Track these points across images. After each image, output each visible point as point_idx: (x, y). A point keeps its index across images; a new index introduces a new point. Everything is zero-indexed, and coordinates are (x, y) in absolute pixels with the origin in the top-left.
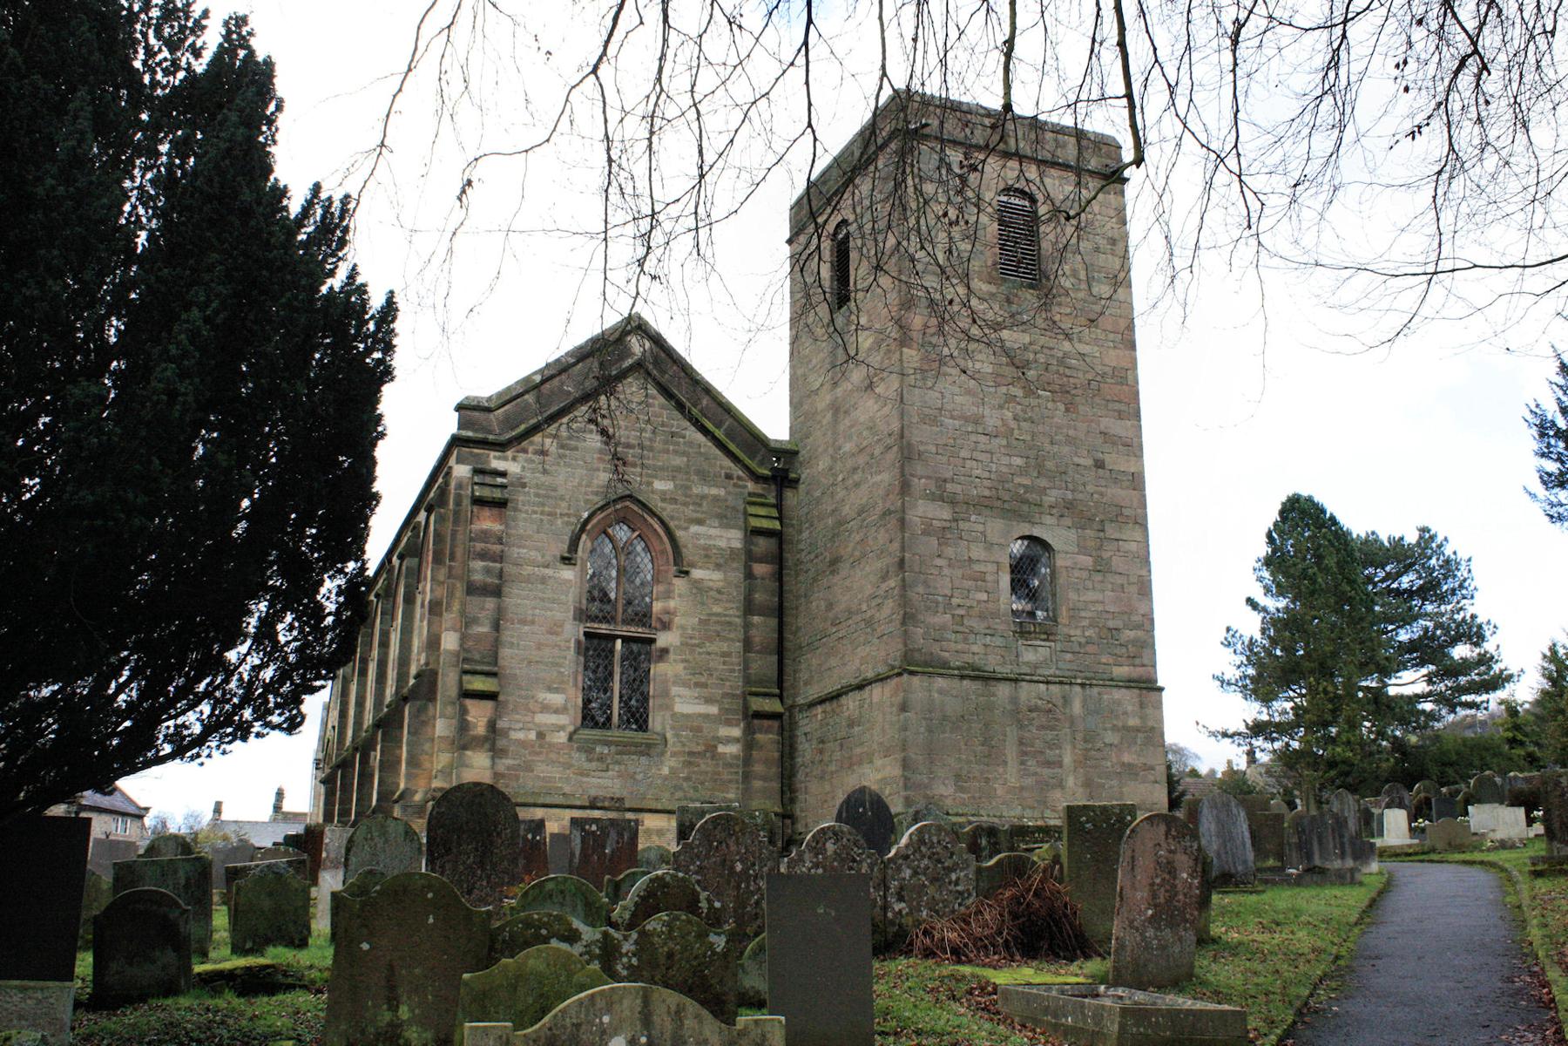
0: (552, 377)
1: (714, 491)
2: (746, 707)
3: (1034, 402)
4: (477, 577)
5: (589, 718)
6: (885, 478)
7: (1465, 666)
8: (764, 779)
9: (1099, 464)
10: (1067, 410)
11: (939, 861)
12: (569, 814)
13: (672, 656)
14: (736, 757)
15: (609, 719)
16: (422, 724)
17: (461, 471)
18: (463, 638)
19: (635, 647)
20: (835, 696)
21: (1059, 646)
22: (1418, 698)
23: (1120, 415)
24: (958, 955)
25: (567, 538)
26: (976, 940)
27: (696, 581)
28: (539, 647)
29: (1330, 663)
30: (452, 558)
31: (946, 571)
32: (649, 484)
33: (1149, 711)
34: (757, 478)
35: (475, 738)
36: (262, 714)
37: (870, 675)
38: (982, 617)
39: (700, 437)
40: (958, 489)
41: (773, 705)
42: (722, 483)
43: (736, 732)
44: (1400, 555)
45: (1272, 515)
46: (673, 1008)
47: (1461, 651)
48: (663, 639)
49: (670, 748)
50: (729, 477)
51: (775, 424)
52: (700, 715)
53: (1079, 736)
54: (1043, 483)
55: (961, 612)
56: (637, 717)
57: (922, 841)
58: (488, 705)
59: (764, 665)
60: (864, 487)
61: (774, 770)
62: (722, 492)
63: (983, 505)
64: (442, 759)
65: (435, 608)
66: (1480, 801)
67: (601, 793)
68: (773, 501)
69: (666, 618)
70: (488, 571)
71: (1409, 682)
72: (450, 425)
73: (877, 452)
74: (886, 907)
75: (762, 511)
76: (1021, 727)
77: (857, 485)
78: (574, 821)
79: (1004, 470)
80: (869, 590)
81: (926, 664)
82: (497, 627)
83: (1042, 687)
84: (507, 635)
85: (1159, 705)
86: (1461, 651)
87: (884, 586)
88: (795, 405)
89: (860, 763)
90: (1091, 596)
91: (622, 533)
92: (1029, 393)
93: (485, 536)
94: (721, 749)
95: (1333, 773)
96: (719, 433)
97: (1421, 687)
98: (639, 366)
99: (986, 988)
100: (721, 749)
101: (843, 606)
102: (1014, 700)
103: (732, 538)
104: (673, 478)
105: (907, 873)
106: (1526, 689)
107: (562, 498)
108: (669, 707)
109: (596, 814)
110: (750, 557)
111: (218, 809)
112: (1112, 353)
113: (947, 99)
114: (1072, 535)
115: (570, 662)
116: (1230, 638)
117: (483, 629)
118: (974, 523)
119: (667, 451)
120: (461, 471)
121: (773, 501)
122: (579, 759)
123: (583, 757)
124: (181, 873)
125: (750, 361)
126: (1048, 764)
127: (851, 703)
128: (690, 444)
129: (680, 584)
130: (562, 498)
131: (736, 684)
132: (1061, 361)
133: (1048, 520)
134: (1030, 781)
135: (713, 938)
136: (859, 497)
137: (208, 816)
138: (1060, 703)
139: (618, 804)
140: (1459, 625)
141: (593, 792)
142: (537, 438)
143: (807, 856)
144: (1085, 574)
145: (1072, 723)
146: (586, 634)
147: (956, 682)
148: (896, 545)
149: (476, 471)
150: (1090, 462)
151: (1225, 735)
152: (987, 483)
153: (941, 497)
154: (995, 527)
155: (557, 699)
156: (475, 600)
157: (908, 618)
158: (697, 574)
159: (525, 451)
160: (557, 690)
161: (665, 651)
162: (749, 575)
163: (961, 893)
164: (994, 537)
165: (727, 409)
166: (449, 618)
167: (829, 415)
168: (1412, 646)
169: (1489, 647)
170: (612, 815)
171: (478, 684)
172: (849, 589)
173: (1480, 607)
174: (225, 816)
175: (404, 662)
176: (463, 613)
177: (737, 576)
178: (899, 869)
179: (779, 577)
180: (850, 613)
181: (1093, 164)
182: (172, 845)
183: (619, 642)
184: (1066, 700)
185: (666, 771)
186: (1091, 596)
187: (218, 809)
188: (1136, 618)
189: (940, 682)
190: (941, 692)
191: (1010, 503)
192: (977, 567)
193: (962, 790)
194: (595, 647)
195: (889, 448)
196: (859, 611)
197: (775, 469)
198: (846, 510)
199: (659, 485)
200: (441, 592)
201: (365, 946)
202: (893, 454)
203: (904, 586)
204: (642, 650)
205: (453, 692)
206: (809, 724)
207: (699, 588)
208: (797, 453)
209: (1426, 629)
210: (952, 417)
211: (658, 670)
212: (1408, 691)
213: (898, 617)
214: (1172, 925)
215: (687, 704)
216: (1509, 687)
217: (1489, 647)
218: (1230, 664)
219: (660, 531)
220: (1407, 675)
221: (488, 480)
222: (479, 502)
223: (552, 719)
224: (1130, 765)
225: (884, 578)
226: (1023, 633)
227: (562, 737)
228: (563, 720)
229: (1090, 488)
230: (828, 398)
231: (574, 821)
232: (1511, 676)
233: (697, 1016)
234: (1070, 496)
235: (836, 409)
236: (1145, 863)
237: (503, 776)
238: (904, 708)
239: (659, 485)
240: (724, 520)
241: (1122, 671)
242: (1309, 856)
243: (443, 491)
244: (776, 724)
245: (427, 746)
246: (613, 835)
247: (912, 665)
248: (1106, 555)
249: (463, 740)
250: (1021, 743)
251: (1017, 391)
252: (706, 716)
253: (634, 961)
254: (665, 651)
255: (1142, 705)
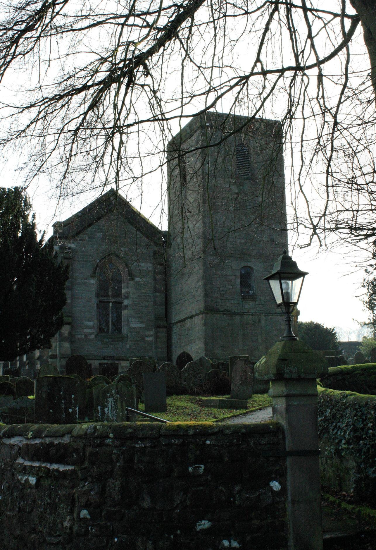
5: (101, 330)
9: (272, 240)
12: (99, 362)
13: (129, 308)
14: (152, 341)
15: (108, 330)
24: (198, 394)
27: (137, 282)
31: (218, 279)
37: (194, 314)
43: (152, 333)
48: (126, 302)
55: (223, 293)
57: (190, 366)
59: (161, 310)
67: (106, 355)
69: (126, 295)
87: (198, 284)
89: (191, 343)
94: (146, 339)
105: (187, 375)
107: (90, 256)
109: (106, 361)
113: (217, 112)
127: (188, 322)
129: (131, 283)
139: (112, 358)
142: (81, 235)
146: (100, 302)
155: (90, 324)
157: (206, 295)
162: (155, 279)
170: (110, 362)
184: (259, 321)
185: (128, 347)
196: (190, 292)
204: (118, 306)
206: (175, 330)
207: (138, 284)
211: (124, 313)
213: (202, 295)
227: (93, 337)
231: (100, 364)
244: (165, 330)
252: (141, 328)
254: (126, 306)
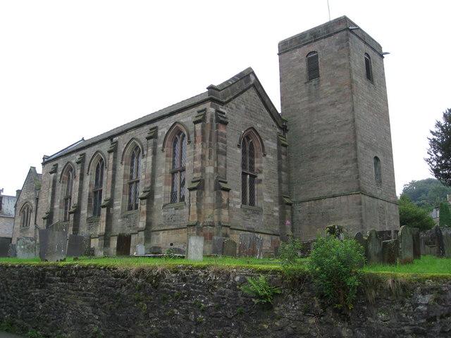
20: (320, 199)
48: (260, 176)
64: (210, 211)
108: (262, 199)
116: (439, 124)
158: (268, 156)
161: (260, 181)
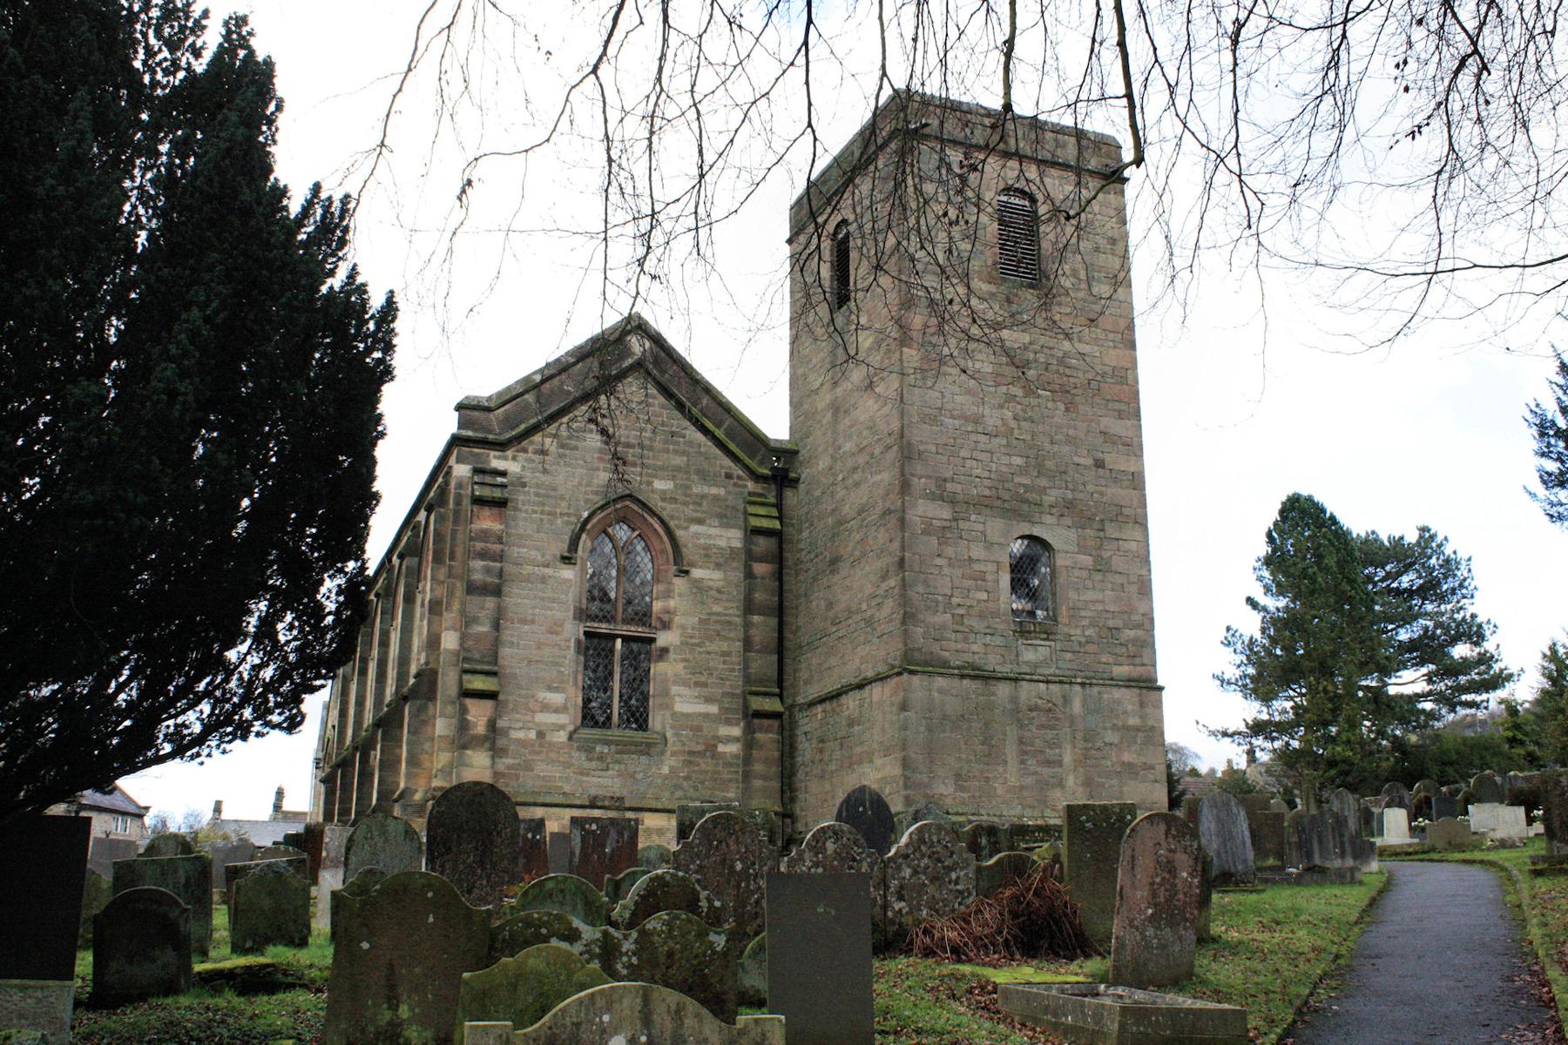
0: (552, 377)
1: (714, 491)
2: (746, 706)
3: (1034, 401)
4: (477, 577)
5: (589, 718)
6: (885, 477)
7: (1465, 665)
8: (764, 778)
9: (1099, 464)
10: (1067, 410)
11: (939, 860)
12: (569, 813)
13: (672, 656)
14: (736, 756)
15: (609, 718)
16: (422, 723)
17: (461, 471)
18: (463, 638)
19: (635, 646)
20: (835, 696)
21: (1059, 646)
22: (1418, 697)
23: (1120, 415)
24: (958, 954)
25: (567, 538)
26: (976, 939)
27: (696, 581)
28: (539, 646)
29: (1330, 662)
30: (452, 558)
31: (946, 571)
32: (649, 483)
33: (1149, 710)
34: (757, 477)
35: (475, 737)
36: (262, 713)
37: (870, 674)
38: (982, 616)
39: (700, 437)
40: (958, 488)
41: (773, 705)
42: (722, 483)
43: (736, 731)
44: (1400, 555)
45: (1272, 515)
46: (673, 1007)
47: (1461, 651)
48: (663, 639)
49: (670, 747)
50: (729, 476)
51: (775, 423)
52: (700, 714)
53: (1079, 735)
54: (1043, 482)
55: (961, 611)
56: (637, 717)
57: (922, 841)
58: (488, 704)
59: (764, 664)
60: (864, 487)
61: (774, 770)
62: (722, 492)
63: (983, 505)
64: (442, 758)
65: (435, 608)
66: (1480, 801)
67: (601, 792)
68: (773, 500)
69: (666, 617)
70: (488, 570)
71: (1409, 682)
72: (450, 425)
73: (877, 452)
74: (886, 906)
75: (762, 511)
76: (1021, 726)
77: (857, 484)
78: (574, 820)
79: (1004, 469)
80: (869, 589)
81: (926, 664)
82: (497, 626)
83: (1042, 686)
84: (507, 634)
85: (1159, 705)
86: (1461, 651)
87: (884, 586)
88: (795, 404)
89: (860, 762)
90: (1091, 595)
91: (622, 533)
92: (1029, 392)
93: (485, 535)
94: (721, 748)
95: (1333, 772)
96: (719, 433)
97: (1421, 687)
98: (639, 365)
99: (986, 987)
100: (721, 748)
101: (843, 606)
102: (1014, 700)
103: (732, 538)
104: (673, 478)
105: (907, 872)
106: (1526, 689)
107: (562, 498)
108: (669, 707)
109: (596, 813)
110: (750, 556)
111: (218, 808)
112: (1112, 352)
113: (947, 99)
114: (1072, 534)
115: (570, 661)
117: (483, 628)
118: (974, 522)
119: (667, 451)
120: (461, 471)
121: (773, 500)
122: (579, 758)
123: (583, 756)
124: (181, 873)
125: (750, 360)
126: (1048, 763)
127: (851, 702)
128: (690, 443)
129: (680, 584)
130: (562, 498)
131: (736, 683)
132: (1061, 361)
133: (1048, 519)
134: (1030, 780)
135: (713, 937)
136: (859, 497)
137: (208, 815)
138: (1060, 702)
139: (618, 803)
140: (1459, 624)
141: (593, 792)
142: (537, 438)
143: (807, 855)
144: (1085, 574)
145: (1072, 723)
146: (586, 633)
147: (956, 681)
148: (896, 545)
149: (476, 471)
150: (1090, 462)
151: (1225, 734)
152: (987, 483)
153: (941, 497)
154: (995, 527)
155: (557, 698)
156: (475, 600)
157: (908, 618)
158: (697, 573)
159: (525, 451)
160: (557, 690)
161: (665, 651)
162: (749, 575)
163: (961, 892)
164: (994, 536)
165: (727, 409)
166: (449, 617)
167: (829, 415)
168: (1412, 645)
169: (1489, 646)
170: (612, 814)
171: (478, 683)
172: (849, 588)
173: (1480, 607)
174: (225, 816)
175: (404, 661)
176: (463, 612)
177: (737, 575)
178: (899, 868)
179: (779, 576)
180: (850, 612)
181: (1093, 164)
182: (172, 844)
183: (619, 641)
184: (1066, 699)
185: (666, 770)
186: (1091, 595)
187: (218, 808)
188: (1136, 618)
189: (940, 682)
190: (941, 691)
191: (1010, 503)
192: (977, 567)
193: (962, 789)
194: (595, 646)
195: (889, 447)
196: (859, 611)
197: (775, 469)
198: (846, 509)
199: (659, 485)
200: (441, 592)
201: (365, 945)
202: (893, 454)
203: (904, 585)
204: (642, 650)
205: (453, 691)
206: (809, 724)
207: (699, 587)
208: (797, 452)
209: (1426, 629)
210: (952, 417)
211: (658, 669)
212: (1408, 690)
213: (898, 617)
214: (1172, 924)
215: (687, 703)
216: (1509, 686)
217: (1489, 646)
218: (1230, 663)
219: (660, 530)
220: (1407, 675)
221: (488, 479)
222: (479, 501)
223: (552, 718)
224: (1130, 765)
225: (884, 577)
226: (1023, 632)
227: (562, 737)
228: (563, 719)
229: (1090, 488)
230: (828, 398)
231: (574, 820)
232: (1511, 675)
233: (697, 1015)
234: (1070, 495)
235: (836, 409)
236: (1145, 862)
237: (503, 775)
238: (904, 707)
239: (659, 485)
240: (724, 520)
241: (1122, 671)
242: (1309, 856)
243: (443, 491)
244: (776, 723)
245: (427, 746)
246: (613, 834)
247: (912, 664)
248: (1106, 555)
249: (463, 739)
250: (1021, 742)
251: (1017, 391)
252: (706, 716)
253: (634, 960)
254: (665, 650)
255: (1142, 704)
